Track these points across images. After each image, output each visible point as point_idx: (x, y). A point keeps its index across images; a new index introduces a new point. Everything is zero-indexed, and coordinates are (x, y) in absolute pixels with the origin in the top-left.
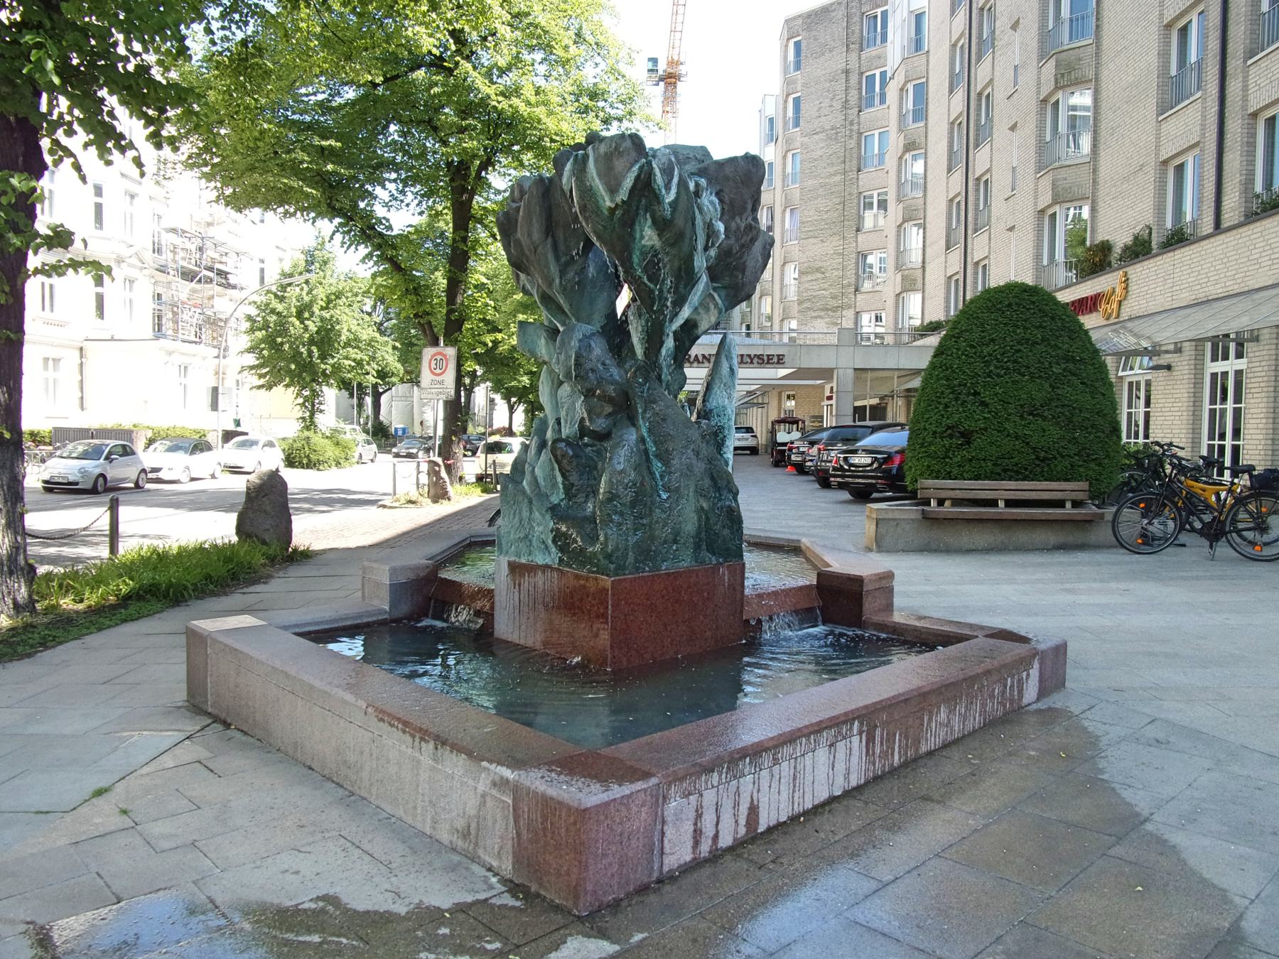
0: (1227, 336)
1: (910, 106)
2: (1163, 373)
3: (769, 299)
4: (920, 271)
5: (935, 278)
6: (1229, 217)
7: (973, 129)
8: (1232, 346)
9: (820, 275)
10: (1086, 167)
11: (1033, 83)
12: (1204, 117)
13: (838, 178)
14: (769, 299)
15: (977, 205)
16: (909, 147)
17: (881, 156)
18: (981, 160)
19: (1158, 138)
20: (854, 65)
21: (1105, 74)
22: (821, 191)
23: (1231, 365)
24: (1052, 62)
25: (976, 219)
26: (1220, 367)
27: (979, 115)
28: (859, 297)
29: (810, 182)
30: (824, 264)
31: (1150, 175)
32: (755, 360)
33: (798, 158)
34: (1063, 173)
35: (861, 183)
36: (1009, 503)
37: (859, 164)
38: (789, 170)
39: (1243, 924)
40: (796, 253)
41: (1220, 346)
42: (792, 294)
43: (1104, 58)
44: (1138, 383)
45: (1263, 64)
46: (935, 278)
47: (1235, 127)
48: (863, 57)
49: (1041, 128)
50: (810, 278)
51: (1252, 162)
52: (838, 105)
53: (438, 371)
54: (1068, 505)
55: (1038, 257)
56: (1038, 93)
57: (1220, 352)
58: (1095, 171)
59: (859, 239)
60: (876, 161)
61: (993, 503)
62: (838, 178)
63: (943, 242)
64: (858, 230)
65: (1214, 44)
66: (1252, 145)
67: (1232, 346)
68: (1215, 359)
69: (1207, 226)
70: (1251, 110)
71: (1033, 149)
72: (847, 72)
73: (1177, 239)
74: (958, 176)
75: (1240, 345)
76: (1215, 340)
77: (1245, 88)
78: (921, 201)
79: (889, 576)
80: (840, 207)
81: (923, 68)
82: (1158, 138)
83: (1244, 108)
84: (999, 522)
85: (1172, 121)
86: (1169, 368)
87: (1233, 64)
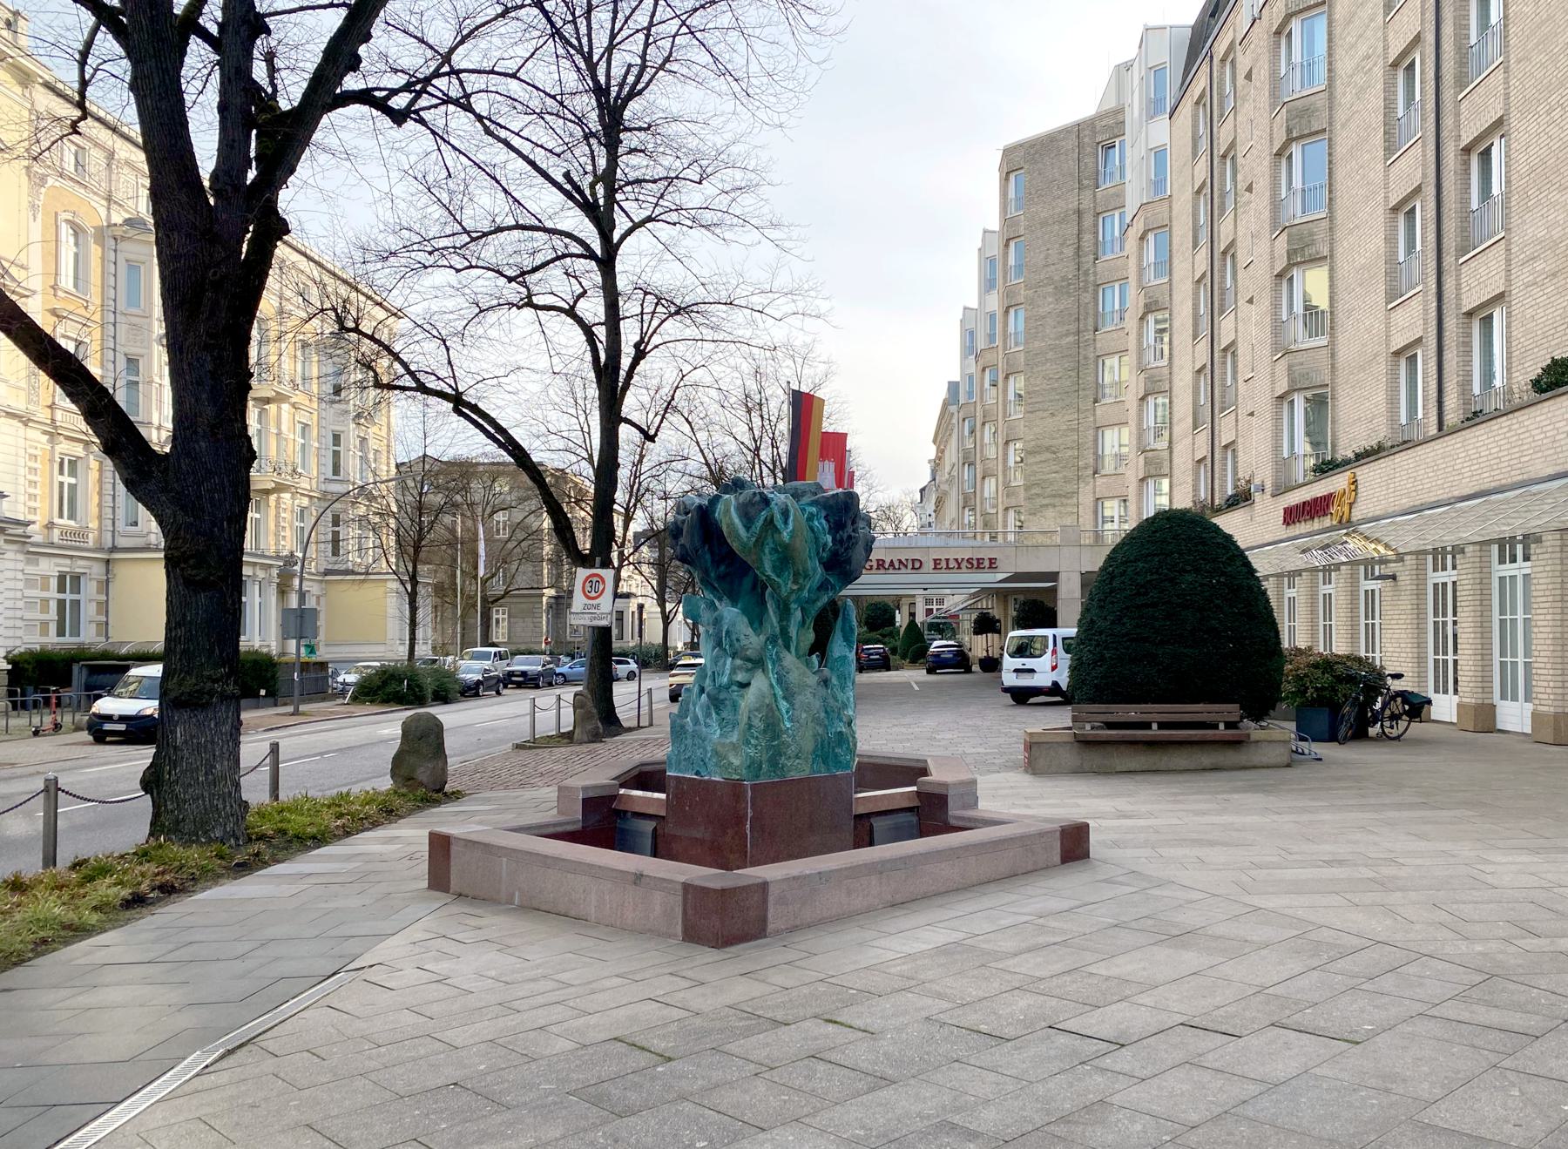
0: (1444, 548)
1: (1152, 259)
2: (1389, 582)
3: (993, 480)
4: (1166, 453)
5: (1183, 461)
6: (1451, 418)
7: (1215, 294)
8: (1519, 548)
9: (1048, 455)
10: (1324, 351)
11: (1266, 257)
12: (1426, 310)
13: (1071, 339)
14: (993, 480)
15: (1224, 380)
16: (1149, 309)
17: (1122, 311)
18: (1227, 329)
19: (1388, 326)
20: (1087, 204)
21: (1339, 251)
22: (1050, 355)
23: (1519, 569)
24: (1284, 236)
25: (1223, 396)
26: (1508, 569)
27: (1223, 277)
28: (1099, 481)
29: (1037, 344)
30: (1055, 442)
31: (1382, 367)
32: (964, 564)
33: (1021, 314)
34: (1299, 358)
35: (1099, 345)
36: (1162, 726)
37: (1096, 323)
38: (1011, 329)
39: (567, 726)
40: (1021, 430)
41: (1507, 548)
42: (1018, 480)
43: (1338, 235)
44: (1444, 584)
45: (1473, 264)
46: (1183, 461)
47: (1451, 323)
48: (1099, 195)
49: (1276, 306)
50: (1038, 458)
51: (1469, 363)
52: (1069, 252)
53: (593, 594)
54: (1155, 726)
55: (1277, 448)
56: (1272, 267)
57: (1506, 555)
58: (1333, 355)
59: (1098, 412)
60: (1117, 317)
61: (1147, 726)
62: (1071, 339)
63: (1190, 420)
64: (1096, 401)
65: (1432, 237)
66: (1467, 344)
67: (1519, 548)
68: (1502, 562)
69: (1433, 430)
70: (1465, 310)
71: (1268, 330)
72: (1079, 212)
73: (1406, 445)
74: (1204, 346)
75: (1526, 548)
76: (1501, 543)
77: (1458, 287)
78: (1166, 371)
79: (974, 782)
80: (1074, 374)
81: (1166, 215)
82: (1388, 326)
83: (1458, 306)
84: (1153, 744)
85: (1400, 310)
86: (1394, 577)
87: (1448, 260)
